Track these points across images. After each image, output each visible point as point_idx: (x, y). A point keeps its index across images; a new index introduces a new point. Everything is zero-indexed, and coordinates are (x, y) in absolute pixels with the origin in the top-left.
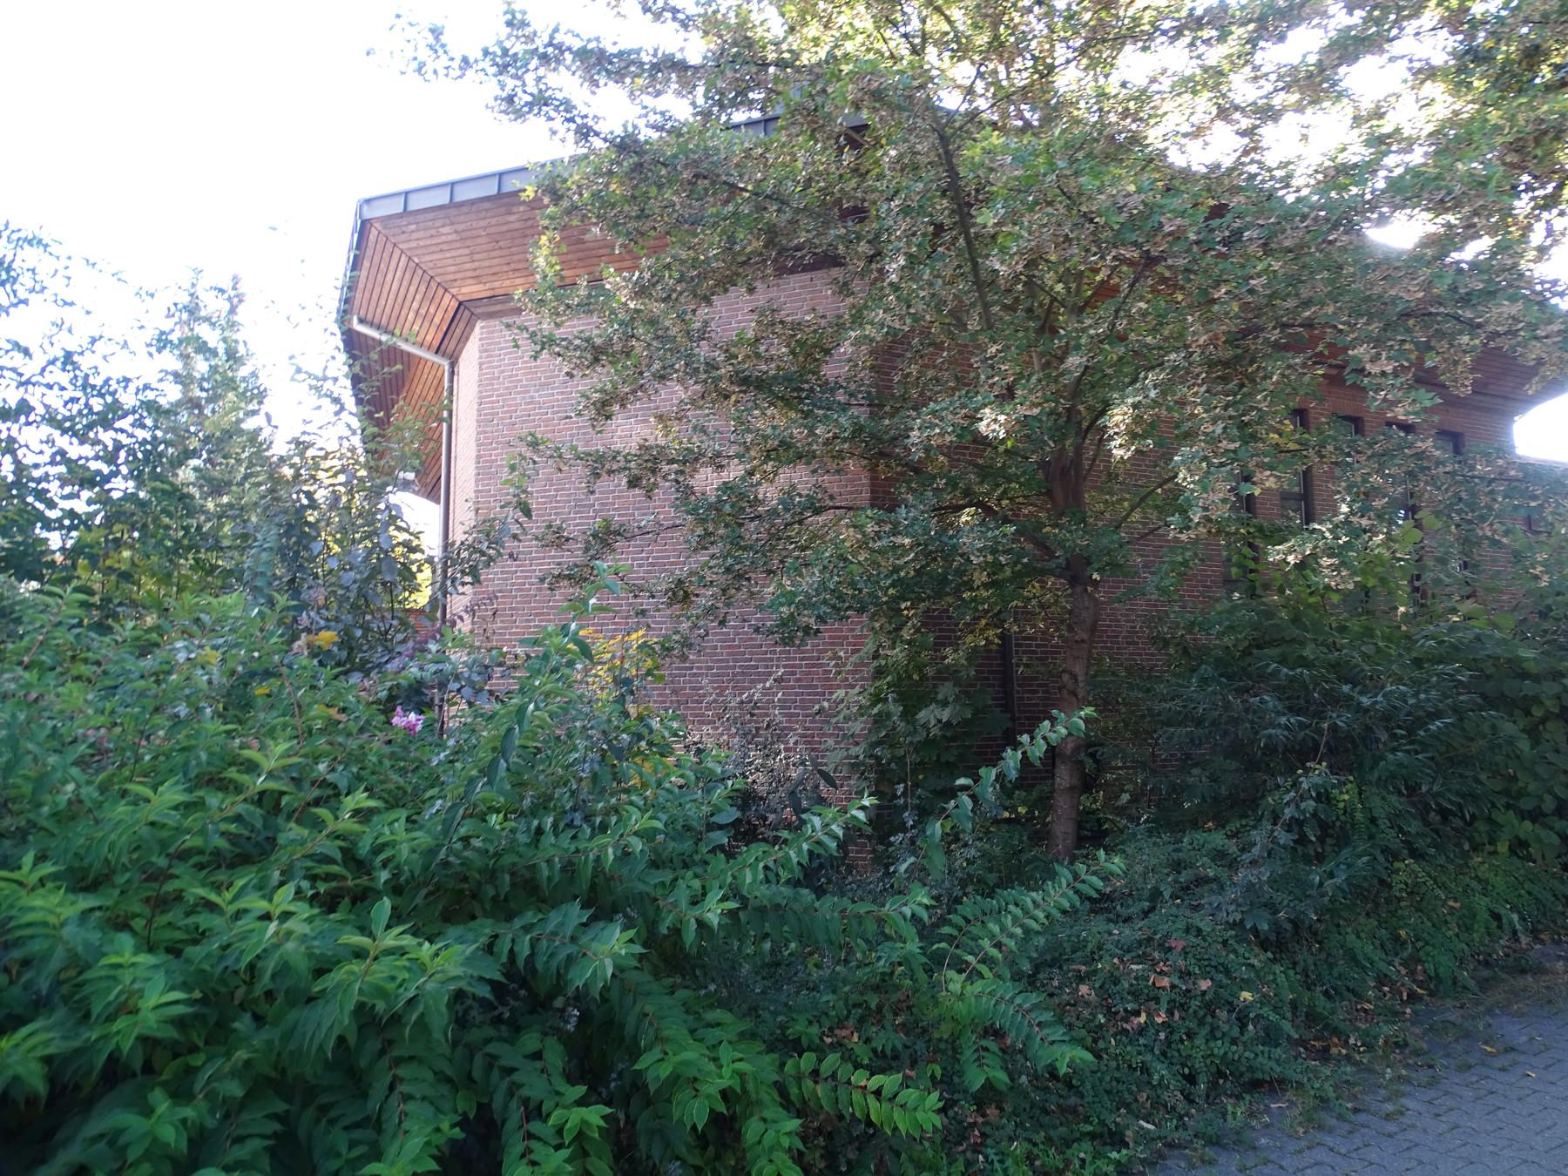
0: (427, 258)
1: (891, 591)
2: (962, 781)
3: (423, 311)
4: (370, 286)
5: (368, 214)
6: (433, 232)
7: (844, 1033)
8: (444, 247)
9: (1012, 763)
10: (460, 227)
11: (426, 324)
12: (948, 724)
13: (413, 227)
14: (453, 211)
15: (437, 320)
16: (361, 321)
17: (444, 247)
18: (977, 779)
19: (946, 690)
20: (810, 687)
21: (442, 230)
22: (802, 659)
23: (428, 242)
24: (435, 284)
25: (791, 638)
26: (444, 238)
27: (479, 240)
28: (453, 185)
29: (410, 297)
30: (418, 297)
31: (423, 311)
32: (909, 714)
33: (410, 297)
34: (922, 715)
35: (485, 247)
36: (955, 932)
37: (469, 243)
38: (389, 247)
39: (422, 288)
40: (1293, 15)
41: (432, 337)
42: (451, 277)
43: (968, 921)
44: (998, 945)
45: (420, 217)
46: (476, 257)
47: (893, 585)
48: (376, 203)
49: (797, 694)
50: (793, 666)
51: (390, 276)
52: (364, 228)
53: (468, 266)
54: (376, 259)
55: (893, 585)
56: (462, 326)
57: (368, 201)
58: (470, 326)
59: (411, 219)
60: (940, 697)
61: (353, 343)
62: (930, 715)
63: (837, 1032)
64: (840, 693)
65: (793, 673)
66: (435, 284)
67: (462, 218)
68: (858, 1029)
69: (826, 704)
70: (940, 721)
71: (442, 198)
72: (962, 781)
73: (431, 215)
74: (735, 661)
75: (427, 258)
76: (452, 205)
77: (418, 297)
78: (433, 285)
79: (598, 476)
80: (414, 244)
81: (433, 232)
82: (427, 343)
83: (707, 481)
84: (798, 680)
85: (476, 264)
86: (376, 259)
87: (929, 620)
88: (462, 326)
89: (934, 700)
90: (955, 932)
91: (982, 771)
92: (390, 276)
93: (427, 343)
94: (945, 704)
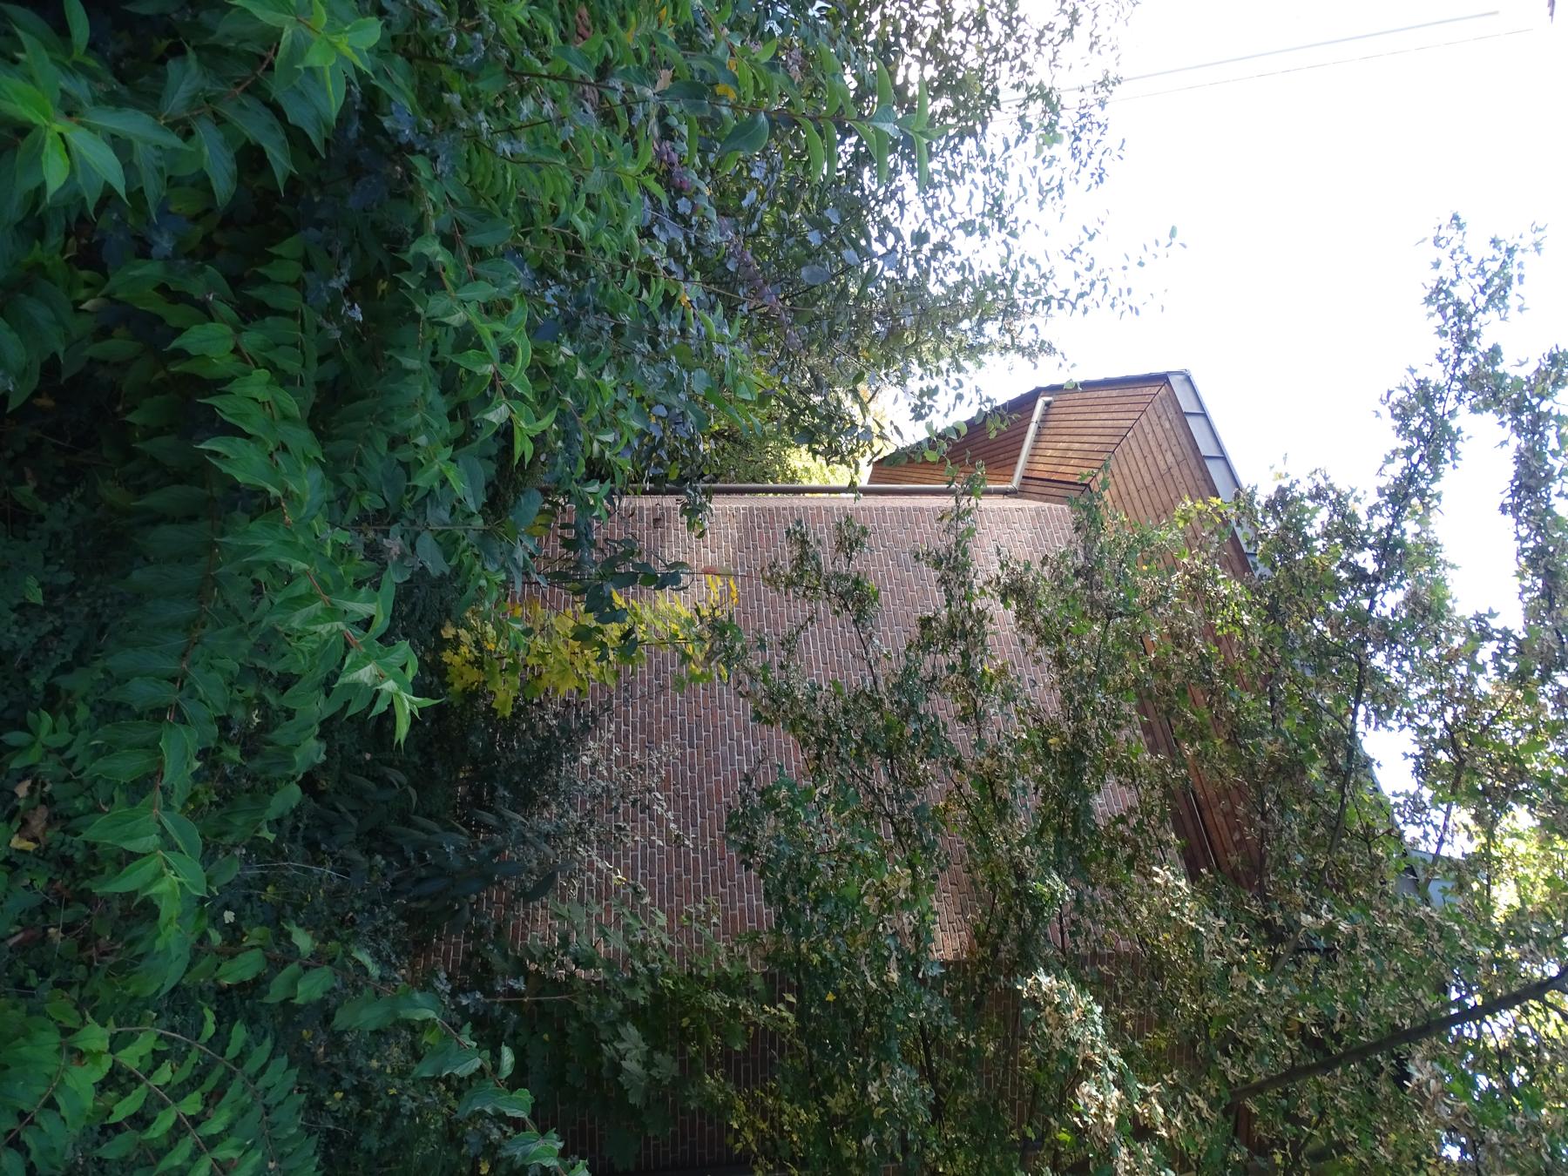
0: (1134, 444)
1: (816, 958)
2: (508, 1057)
3: (1070, 454)
4: (1090, 402)
5: (1172, 379)
6: (1165, 446)
7: (38, 823)
8: (1150, 460)
9: (534, 1148)
10: (1175, 471)
11: (1055, 461)
12: (617, 1069)
13: (1167, 425)
14: (1193, 463)
15: (1062, 469)
16: (1048, 404)
17: (1150, 460)
18: (514, 1084)
19: (667, 1066)
20: (671, 893)
21: (1169, 456)
22: (705, 881)
23: (1152, 443)
24: (1106, 458)
25: (736, 828)
26: (1159, 458)
27: (1163, 494)
28: (1224, 458)
29: (1085, 439)
30: (1086, 446)
31: (1070, 454)
32: (633, 1013)
33: (1085, 439)
34: (631, 1032)
35: (1156, 500)
36: (232, 1051)
37: (1159, 483)
38: (1141, 407)
39: (1098, 447)
40: (125, 1164)
41: (1041, 469)
42: (1116, 471)
43: (254, 1079)
44: (178, 1130)
45: (1179, 431)
46: (1144, 493)
47: (824, 960)
48: (1187, 387)
49: (661, 876)
50: (696, 870)
51: (1105, 416)
52: (1162, 379)
53: (1131, 486)
54: (1124, 400)
55: (824, 960)
56: (1060, 492)
57: (1188, 379)
58: (1063, 499)
59: (1176, 422)
60: (658, 1056)
61: (1024, 404)
62: (631, 1047)
63: (43, 812)
64: (662, 920)
65: (687, 871)
66: (1106, 458)
67: (1186, 471)
68: (43, 854)
69: (647, 900)
70: (623, 1058)
71: (1206, 448)
72: (508, 1057)
73: (1184, 440)
74: (702, 798)
75: (1134, 444)
76: (1201, 460)
77: (1086, 446)
78: (1105, 456)
79: (938, 564)
80: (1147, 429)
81: (1165, 446)
82: (1034, 466)
83: (942, 707)
84: (679, 877)
85: (1135, 494)
86: (1124, 400)
87: (765, 1039)
88: (1060, 492)
89: (655, 1048)
90: (232, 1051)
91: (525, 1095)
92: (1105, 416)
93: (1034, 466)
94: (648, 1064)
